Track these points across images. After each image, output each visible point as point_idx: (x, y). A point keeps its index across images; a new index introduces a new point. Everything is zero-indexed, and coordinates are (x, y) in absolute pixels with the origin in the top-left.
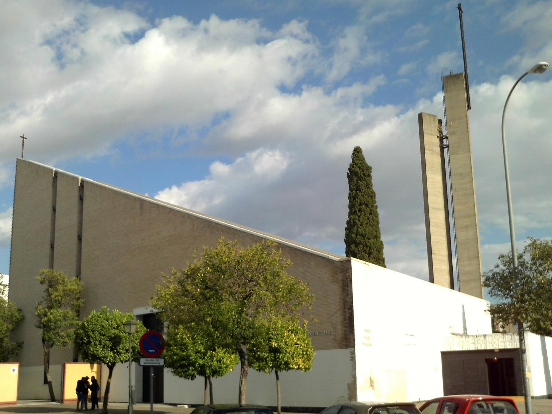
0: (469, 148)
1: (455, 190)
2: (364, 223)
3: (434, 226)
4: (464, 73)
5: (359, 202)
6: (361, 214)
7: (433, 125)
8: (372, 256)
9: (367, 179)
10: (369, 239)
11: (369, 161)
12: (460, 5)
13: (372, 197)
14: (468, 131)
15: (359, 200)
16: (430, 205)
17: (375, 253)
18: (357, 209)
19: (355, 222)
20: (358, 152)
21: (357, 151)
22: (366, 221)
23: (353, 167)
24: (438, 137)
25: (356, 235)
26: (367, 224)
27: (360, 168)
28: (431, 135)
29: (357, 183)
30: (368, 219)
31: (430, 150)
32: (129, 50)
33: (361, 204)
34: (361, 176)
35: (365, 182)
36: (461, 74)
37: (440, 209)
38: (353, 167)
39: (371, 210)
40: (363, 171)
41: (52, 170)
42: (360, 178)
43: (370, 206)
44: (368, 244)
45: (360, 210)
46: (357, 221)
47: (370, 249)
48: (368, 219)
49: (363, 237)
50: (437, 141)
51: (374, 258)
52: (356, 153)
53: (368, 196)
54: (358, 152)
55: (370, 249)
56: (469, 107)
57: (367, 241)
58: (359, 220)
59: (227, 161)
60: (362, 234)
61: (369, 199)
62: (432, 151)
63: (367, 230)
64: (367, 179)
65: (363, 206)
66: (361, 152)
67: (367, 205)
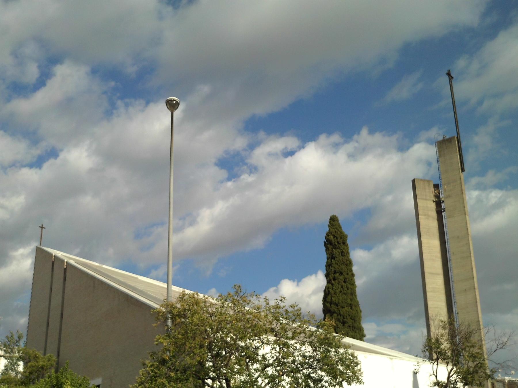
0: (465, 210)
1: (453, 253)
2: (337, 291)
3: (431, 292)
4: (456, 136)
5: (333, 270)
6: (335, 283)
7: (427, 190)
8: (346, 325)
9: (342, 247)
10: (343, 307)
11: (345, 230)
12: (449, 71)
13: (347, 265)
14: (462, 193)
15: (333, 268)
16: (426, 270)
17: (350, 322)
18: (331, 278)
19: (329, 291)
20: (334, 221)
21: (333, 220)
22: (339, 290)
23: (328, 236)
24: (434, 201)
25: (331, 304)
26: (341, 292)
27: (334, 236)
28: (426, 199)
29: (332, 251)
30: (342, 287)
31: (425, 215)
32: (288, 160)
33: (335, 272)
34: (335, 244)
35: (340, 251)
36: (454, 137)
37: (438, 274)
38: (328, 236)
39: (345, 279)
40: (337, 238)
41: (63, 261)
42: (334, 247)
43: (344, 274)
44: (342, 313)
45: (334, 279)
46: (330, 290)
47: (344, 318)
48: (342, 287)
49: (337, 305)
50: (433, 205)
51: (350, 326)
52: (332, 222)
53: (342, 264)
54: (334, 221)
55: (344, 318)
57: (341, 309)
58: (333, 289)
59: (368, 248)
60: (335, 303)
61: (344, 267)
62: (428, 216)
63: (341, 298)
64: (342, 247)
65: (338, 274)
66: (337, 221)
67: (341, 273)
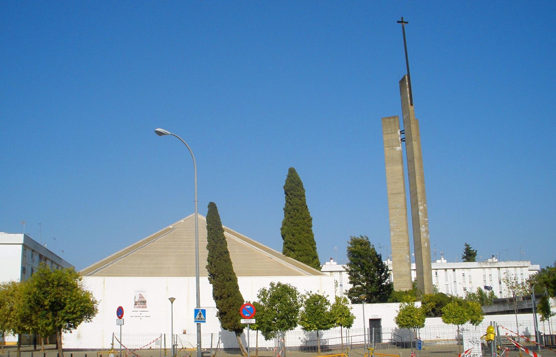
56: (412, 105)
